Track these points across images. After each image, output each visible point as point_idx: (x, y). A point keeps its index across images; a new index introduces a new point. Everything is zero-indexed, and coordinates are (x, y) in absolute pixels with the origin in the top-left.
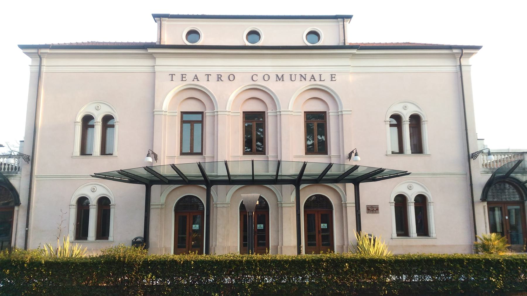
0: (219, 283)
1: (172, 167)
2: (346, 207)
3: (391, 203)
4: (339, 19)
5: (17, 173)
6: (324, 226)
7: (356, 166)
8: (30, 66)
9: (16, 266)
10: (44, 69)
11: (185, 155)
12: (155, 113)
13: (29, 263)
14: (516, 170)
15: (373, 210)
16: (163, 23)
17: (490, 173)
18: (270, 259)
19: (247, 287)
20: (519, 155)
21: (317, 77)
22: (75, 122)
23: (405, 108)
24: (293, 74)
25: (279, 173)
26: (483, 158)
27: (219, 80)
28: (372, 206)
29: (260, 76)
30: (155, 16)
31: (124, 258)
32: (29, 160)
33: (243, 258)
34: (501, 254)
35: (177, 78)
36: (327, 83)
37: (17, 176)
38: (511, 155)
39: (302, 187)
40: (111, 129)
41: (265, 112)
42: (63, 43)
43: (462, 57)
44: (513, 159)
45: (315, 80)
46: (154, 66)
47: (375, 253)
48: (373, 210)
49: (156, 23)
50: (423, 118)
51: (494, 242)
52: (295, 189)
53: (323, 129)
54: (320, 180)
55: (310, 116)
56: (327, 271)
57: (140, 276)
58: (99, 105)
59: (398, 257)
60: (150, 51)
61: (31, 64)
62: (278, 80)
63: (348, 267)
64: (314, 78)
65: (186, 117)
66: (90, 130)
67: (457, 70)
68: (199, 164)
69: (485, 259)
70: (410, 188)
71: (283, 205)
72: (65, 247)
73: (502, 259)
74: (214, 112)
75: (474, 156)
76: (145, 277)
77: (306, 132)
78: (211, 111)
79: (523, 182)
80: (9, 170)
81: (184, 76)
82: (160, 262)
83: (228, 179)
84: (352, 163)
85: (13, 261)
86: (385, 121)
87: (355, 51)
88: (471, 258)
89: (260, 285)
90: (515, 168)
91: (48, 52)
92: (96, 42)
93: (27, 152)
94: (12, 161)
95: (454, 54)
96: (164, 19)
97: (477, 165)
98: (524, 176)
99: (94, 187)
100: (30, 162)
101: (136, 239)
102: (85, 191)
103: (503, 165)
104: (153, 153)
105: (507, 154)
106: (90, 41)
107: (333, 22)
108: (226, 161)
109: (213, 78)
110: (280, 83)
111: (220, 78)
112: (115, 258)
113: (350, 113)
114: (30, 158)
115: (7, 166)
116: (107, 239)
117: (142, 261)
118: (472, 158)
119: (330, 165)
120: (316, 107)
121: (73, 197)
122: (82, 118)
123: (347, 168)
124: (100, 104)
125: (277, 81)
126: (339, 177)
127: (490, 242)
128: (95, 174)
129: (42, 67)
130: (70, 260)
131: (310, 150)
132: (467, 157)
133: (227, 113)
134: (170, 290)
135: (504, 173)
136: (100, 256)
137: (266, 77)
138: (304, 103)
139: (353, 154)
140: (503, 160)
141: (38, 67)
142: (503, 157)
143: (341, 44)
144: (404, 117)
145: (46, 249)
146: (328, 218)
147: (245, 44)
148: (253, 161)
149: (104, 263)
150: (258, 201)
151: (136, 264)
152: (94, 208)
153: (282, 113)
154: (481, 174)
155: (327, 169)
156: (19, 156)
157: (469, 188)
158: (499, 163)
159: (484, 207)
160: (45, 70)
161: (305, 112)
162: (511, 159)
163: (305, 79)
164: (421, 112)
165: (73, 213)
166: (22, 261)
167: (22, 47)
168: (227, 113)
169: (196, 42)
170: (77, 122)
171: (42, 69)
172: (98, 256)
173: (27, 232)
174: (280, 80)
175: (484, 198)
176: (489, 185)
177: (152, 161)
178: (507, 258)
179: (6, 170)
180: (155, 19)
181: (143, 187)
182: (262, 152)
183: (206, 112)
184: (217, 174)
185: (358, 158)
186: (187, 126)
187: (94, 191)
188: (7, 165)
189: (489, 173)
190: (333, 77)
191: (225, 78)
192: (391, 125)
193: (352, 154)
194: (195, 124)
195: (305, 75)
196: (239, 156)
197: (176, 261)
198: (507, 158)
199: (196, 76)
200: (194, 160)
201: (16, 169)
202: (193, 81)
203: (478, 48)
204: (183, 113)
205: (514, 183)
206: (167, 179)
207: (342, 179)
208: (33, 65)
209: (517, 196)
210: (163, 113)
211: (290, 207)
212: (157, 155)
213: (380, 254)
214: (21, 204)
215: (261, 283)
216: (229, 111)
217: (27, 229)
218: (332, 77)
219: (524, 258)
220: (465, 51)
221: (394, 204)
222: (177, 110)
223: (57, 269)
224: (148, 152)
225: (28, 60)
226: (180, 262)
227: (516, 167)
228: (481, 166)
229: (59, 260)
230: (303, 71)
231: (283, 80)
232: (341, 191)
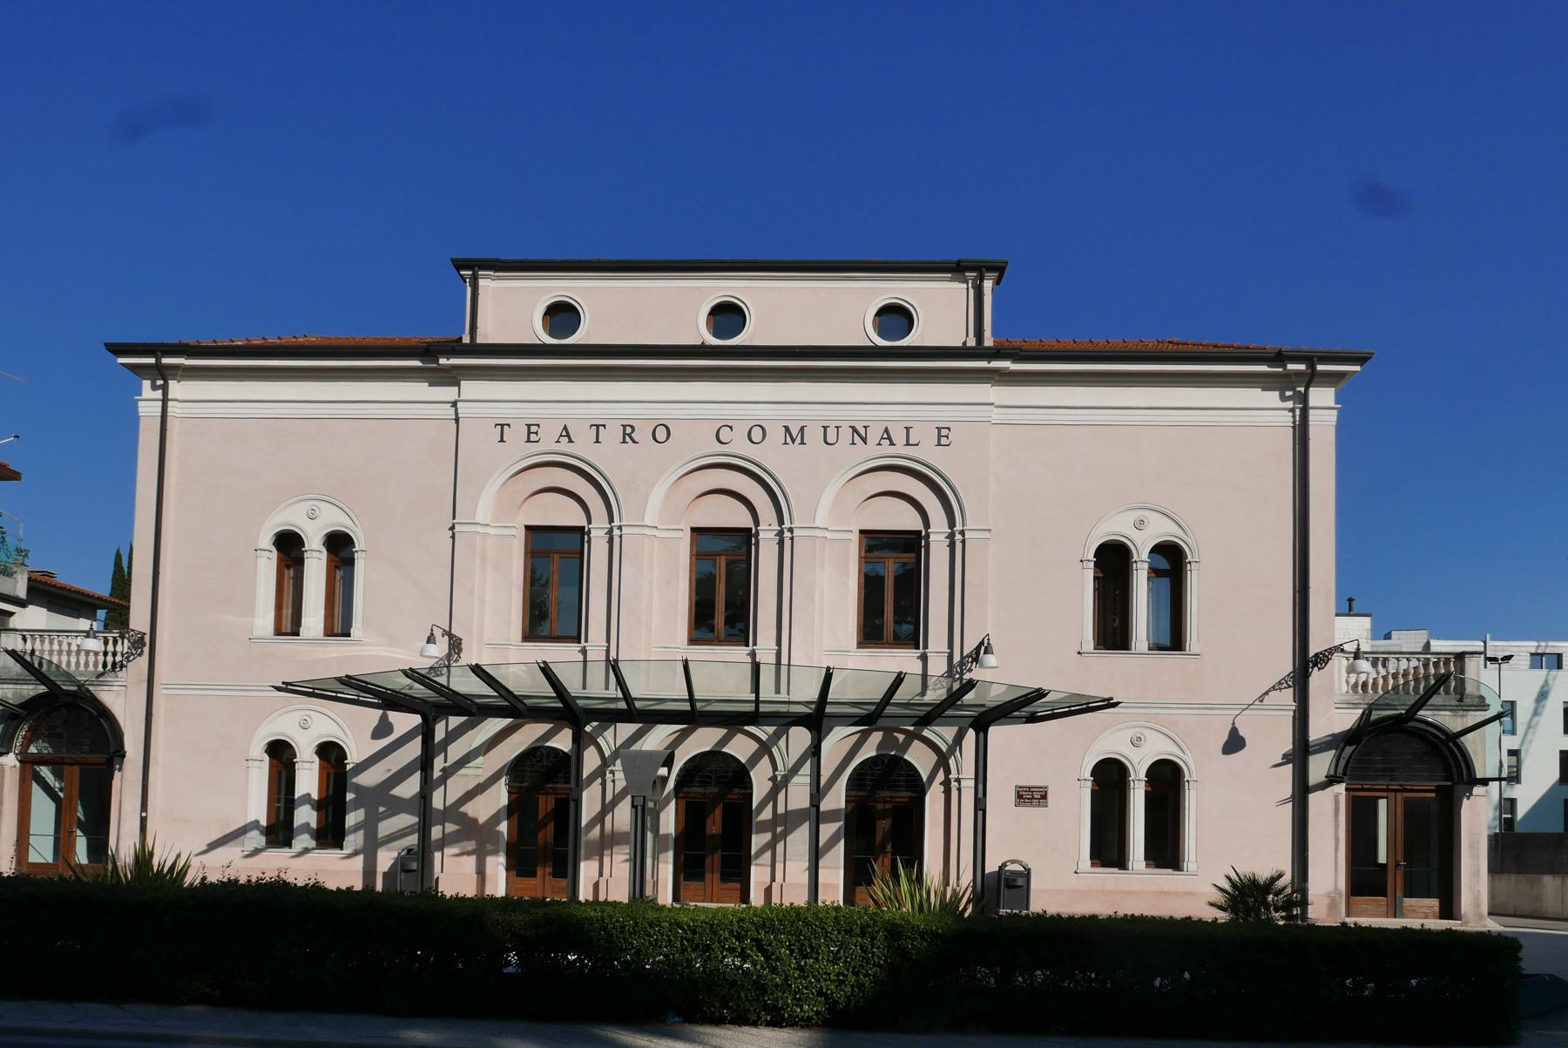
11: (536, 642)
15: (1033, 798)
16: (481, 282)
21: (898, 436)
24: (833, 425)
27: (628, 439)
28: (1029, 788)
36: (927, 453)
37: (117, 684)
48: (1033, 798)
58: (314, 505)
64: (889, 438)
68: (542, 665)
75: (1322, 659)
77: (863, 586)
81: (533, 429)
104: (449, 634)
109: (612, 434)
111: (629, 435)
113: (986, 535)
125: (786, 443)
126: (932, 710)
128: (283, 683)
135: (1403, 707)
137: (757, 432)
153: (796, 532)
161: (861, 532)
163: (865, 441)
164: (1184, 537)
187: (306, 726)
190: (532, 431)
191: (644, 434)
199: (565, 428)
206: (472, 701)
212: (461, 640)
217: (144, 814)
218: (942, 436)
224: (430, 631)
230: (858, 415)
231: (802, 443)
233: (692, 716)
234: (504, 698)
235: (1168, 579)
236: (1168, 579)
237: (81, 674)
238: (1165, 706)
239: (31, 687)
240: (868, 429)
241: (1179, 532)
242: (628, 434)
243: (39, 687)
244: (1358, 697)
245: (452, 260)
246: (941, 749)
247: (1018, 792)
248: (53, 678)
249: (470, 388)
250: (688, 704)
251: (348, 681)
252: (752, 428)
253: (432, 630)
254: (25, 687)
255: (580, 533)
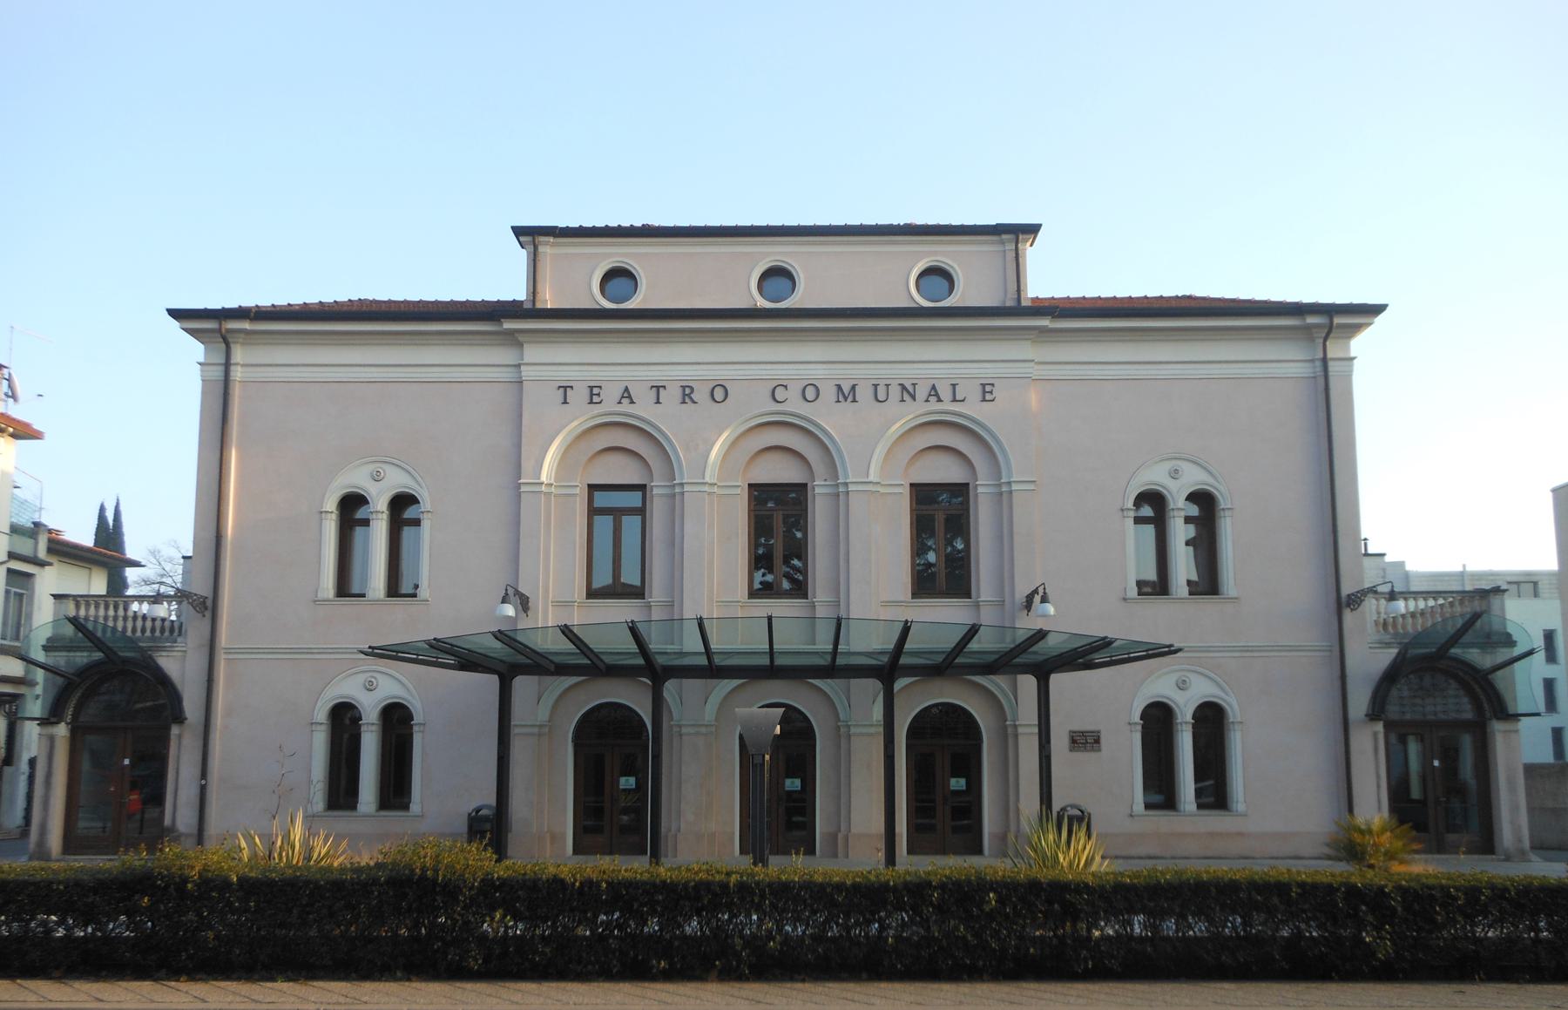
0: (671, 937)
1: (563, 632)
2: (1016, 736)
3: (1133, 726)
4: (1004, 237)
5: (175, 642)
6: (957, 784)
7: (1040, 631)
8: (200, 364)
9: (167, 887)
10: (237, 374)
12: (523, 489)
13: (198, 881)
14: (1467, 638)
16: (541, 249)
17: (1395, 645)
18: (797, 879)
19: (738, 948)
20: (1478, 598)
21: (945, 393)
22: (321, 512)
23: (1175, 474)
25: (839, 647)
26: (1378, 605)
27: (687, 400)
29: (795, 390)
30: (519, 231)
31: (436, 871)
32: (206, 608)
33: (731, 876)
34: (1396, 868)
35: (579, 396)
36: (973, 409)
37: (177, 649)
38: (1453, 597)
39: (900, 684)
40: (413, 529)
41: (807, 484)
42: (286, 304)
43: (1331, 335)
44: (1458, 609)
45: (940, 400)
46: (519, 366)
47: (1071, 864)
49: (524, 250)
50: (1223, 503)
51: (1378, 838)
52: (882, 693)
53: (959, 524)
54: (947, 668)
55: (923, 495)
56: (940, 909)
57: (474, 916)
59: (1122, 877)
60: (508, 325)
61: (202, 360)
62: (841, 399)
63: (993, 902)
64: (937, 395)
65: (602, 500)
66: (359, 531)
67: (1314, 373)
68: (630, 625)
69: (1346, 884)
70: (1182, 686)
71: (853, 730)
72: (292, 837)
73: (1390, 885)
74: (674, 486)
75: (1355, 601)
76: (488, 919)
78: (663, 484)
79: (1484, 670)
80: (155, 631)
81: (596, 391)
82: (524, 881)
83: (707, 663)
84: (1028, 624)
85: (159, 875)
86: (1122, 510)
87: (1045, 322)
88: (1309, 880)
89: (772, 944)
90: (1464, 634)
91: (246, 329)
92: (371, 299)
93: (201, 588)
94: (161, 610)
95: (1308, 328)
96: (542, 239)
97: (1363, 625)
98: (1487, 653)
99: (370, 679)
100: (208, 614)
101: (478, 810)
102: (349, 688)
103: (1429, 624)
104: (517, 593)
105: (1443, 595)
106: (355, 298)
107: (992, 243)
108: (701, 617)
109: (671, 395)
110: (847, 406)
111: (689, 395)
112: (412, 871)
113: (1032, 487)
114: (209, 603)
115: (149, 624)
116: (406, 807)
117: (479, 880)
118: (1348, 605)
119: (973, 630)
120: (943, 471)
121: (319, 704)
122: (338, 501)
123: (1021, 636)
124: (384, 466)
125: (838, 401)
126: (996, 660)
127: (1367, 837)
128: (370, 647)
129: (232, 368)
130: (301, 875)
131: (925, 584)
132: (1333, 606)
133: (706, 488)
134: (548, 950)
136: (377, 864)
137: (809, 392)
138: (908, 463)
139: (1037, 598)
140: (1432, 611)
141: (222, 368)
142: (1431, 603)
143: (1010, 303)
144: (1173, 498)
145: (243, 844)
146: (968, 765)
147: (756, 305)
148: (770, 619)
149: (387, 882)
150: (778, 727)
151: (465, 887)
152: (372, 731)
154: (1370, 648)
155: (969, 637)
156: (179, 597)
157: (1337, 684)
158: (1420, 621)
159: (1375, 734)
160: (239, 374)
162: (1454, 609)
163: (913, 397)
164: (1216, 484)
165: (320, 741)
166: (180, 876)
167: (176, 314)
168: (706, 488)
169: (627, 299)
170: (326, 512)
171: (232, 374)
172: (372, 863)
173: (203, 790)
174: (846, 399)
175: (1377, 711)
176: (1390, 677)
177: (514, 615)
178: (1404, 883)
179: (148, 633)
180: (522, 239)
181: (493, 681)
182: (800, 589)
183: (652, 484)
184: (680, 647)
185: (1050, 609)
186: (604, 524)
188: (149, 619)
189: (1392, 645)
191: (701, 394)
192: (1139, 520)
193: (1033, 597)
194: (624, 518)
195: (914, 385)
196: (738, 602)
197: (562, 881)
198: (1442, 605)
199: (627, 389)
200: (620, 611)
201: (173, 631)
202: (620, 403)
203: (1377, 310)
204: (593, 488)
205: (1461, 674)
207: (1006, 663)
208: (207, 362)
209: (1468, 707)
210: (544, 488)
211: (871, 735)
212: (528, 598)
213: (1081, 866)
214: (186, 719)
215: (773, 939)
216: (712, 481)
217: (203, 782)
218: (986, 392)
219: (1450, 882)
220: (1338, 320)
221: (1139, 728)
222: (578, 480)
223: (269, 895)
225: (195, 350)
226: (574, 884)
227: (1467, 630)
228: (1370, 628)
229: (274, 875)
230: (907, 373)
231: (854, 401)
232: (1005, 695)
233: (770, 670)
234: (585, 655)
235: (1153, 526)
236: (1153, 526)
237: (139, 639)
238: (1207, 649)
239: (85, 654)
240: (957, 386)
241: (1211, 480)
242: (687, 394)
243: (94, 654)
244: (1388, 636)
245: (512, 228)
246: (640, 665)
247: (1073, 737)
248: (110, 645)
249: (533, 353)
250: (705, 657)
251: (438, 645)
252: (775, 388)
253: (506, 590)
254: (79, 654)
255: (801, 488)
